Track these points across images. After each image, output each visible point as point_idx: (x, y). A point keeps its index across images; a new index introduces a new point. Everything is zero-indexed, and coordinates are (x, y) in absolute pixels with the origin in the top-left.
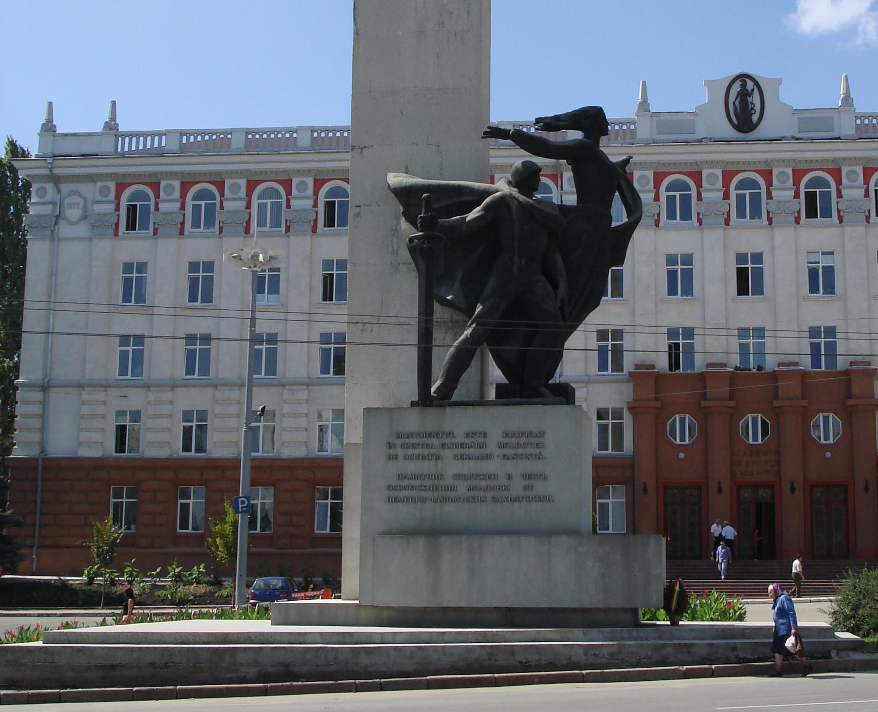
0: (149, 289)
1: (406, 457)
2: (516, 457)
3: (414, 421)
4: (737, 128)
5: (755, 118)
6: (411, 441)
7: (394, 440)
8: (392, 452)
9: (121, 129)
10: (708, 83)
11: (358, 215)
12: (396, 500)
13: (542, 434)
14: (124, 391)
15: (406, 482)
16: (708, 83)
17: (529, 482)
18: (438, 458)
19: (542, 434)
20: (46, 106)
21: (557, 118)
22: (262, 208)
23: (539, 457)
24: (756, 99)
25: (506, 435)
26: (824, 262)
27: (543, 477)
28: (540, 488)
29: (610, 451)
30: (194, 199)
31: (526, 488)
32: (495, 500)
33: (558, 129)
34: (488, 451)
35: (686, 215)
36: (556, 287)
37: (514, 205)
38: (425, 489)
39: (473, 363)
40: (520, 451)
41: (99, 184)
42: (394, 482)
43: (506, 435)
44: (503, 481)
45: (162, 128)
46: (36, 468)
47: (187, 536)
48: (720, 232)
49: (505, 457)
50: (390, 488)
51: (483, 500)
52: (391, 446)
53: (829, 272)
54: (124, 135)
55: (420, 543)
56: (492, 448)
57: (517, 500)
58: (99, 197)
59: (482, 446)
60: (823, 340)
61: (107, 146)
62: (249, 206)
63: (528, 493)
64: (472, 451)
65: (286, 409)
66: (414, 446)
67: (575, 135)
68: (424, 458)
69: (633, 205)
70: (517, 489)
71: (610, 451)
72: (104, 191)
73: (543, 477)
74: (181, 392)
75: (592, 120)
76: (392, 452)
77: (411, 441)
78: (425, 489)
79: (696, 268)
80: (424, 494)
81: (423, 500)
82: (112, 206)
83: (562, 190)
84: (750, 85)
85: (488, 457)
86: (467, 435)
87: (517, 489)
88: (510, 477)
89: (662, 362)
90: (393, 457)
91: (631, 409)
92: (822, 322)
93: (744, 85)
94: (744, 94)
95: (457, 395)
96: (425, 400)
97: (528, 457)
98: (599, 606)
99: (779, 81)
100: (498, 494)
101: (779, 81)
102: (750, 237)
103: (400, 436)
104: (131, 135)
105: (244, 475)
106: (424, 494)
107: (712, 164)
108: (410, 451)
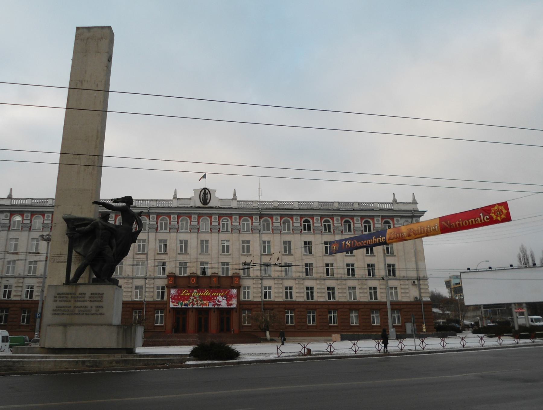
0: (251, 249)
1: (60, 301)
2: (94, 301)
3: (66, 290)
4: (203, 204)
5: (208, 201)
6: (62, 296)
7: (56, 295)
8: (56, 299)
9: (13, 197)
10: (194, 190)
11: (55, 226)
12: (55, 314)
13: (102, 294)
14: (7, 279)
15: (59, 309)
16: (194, 190)
17: (97, 309)
18: (70, 301)
19: (102, 294)
20: (10, 190)
21: (118, 199)
22: (162, 224)
23: (101, 301)
24: (209, 196)
25: (92, 294)
26: (227, 243)
27: (102, 307)
28: (101, 311)
29: (310, 300)
30: (222, 221)
31: (97, 311)
32: (86, 314)
33: (118, 202)
34: (85, 299)
35: (309, 229)
36: (112, 248)
37: (100, 224)
38: (65, 311)
39: (85, 272)
40: (96, 299)
41: (5, 214)
42: (55, 309)
43: (92, 294)
44: (89, 308)
45: (373, 201)
46: (38, 303)
47: (311, 326)
48: (6, 232)
49: (91, 301)
50: (53, 310)
51: (82, 314)
52: (55, 297)
53: (228, 247)
54: (14, 199)
55: (61, 328)
56: (87, 298)
57: (92, 314)
58: (4, 218)
59: (84, 298)
60: (183, 265)
61: (7, 202)
62: (157, 223)
63: (97, 312)
64: (80, 299)
65: (147, 286)
66: (63, 297)
67: (124, 204)
68: (65, 301)
69: (140, 224)
70: (93, 311)
71: (28, 299)
72: (6, 216)
73: (102, 307)
74: (327, 281)
75: (128, 200)
76: (56, 299)
77: (62, 296)
78: (65, 311)
79: (189, 244)
80: (64, 312)
81: (63, 314)
82: (8, 221)
83: (115, 220)
84: (207, 191)
85: (85, 301)
86: (80, 294)
87: (93, 311)
88: (92, 307)
89: (199, 273)
90: (56, 301)
91: (167, 286)
92: (350, 262)
93: (205, 191)
94: (205, 194)
95: (79, 281)
96: (68, 282)
97: (97, 301)
98: (115, 347)
99: (216, 191)
100: (87, 312)
101: (216, 191)
102: (308, 237)
103: (58, 294)
104: (16, 199)
105: (389, 306)
106: (64, 312)
107: (195, 214)
108: (61, 299)
